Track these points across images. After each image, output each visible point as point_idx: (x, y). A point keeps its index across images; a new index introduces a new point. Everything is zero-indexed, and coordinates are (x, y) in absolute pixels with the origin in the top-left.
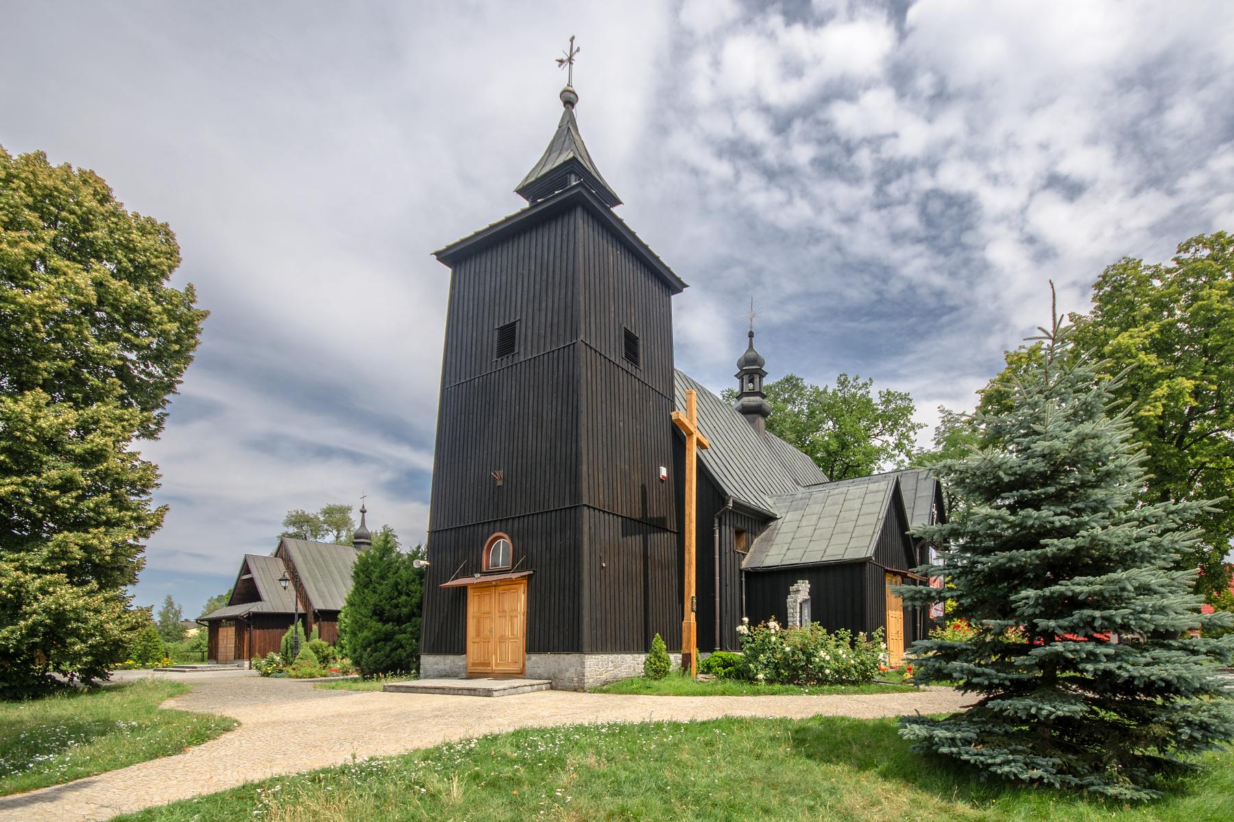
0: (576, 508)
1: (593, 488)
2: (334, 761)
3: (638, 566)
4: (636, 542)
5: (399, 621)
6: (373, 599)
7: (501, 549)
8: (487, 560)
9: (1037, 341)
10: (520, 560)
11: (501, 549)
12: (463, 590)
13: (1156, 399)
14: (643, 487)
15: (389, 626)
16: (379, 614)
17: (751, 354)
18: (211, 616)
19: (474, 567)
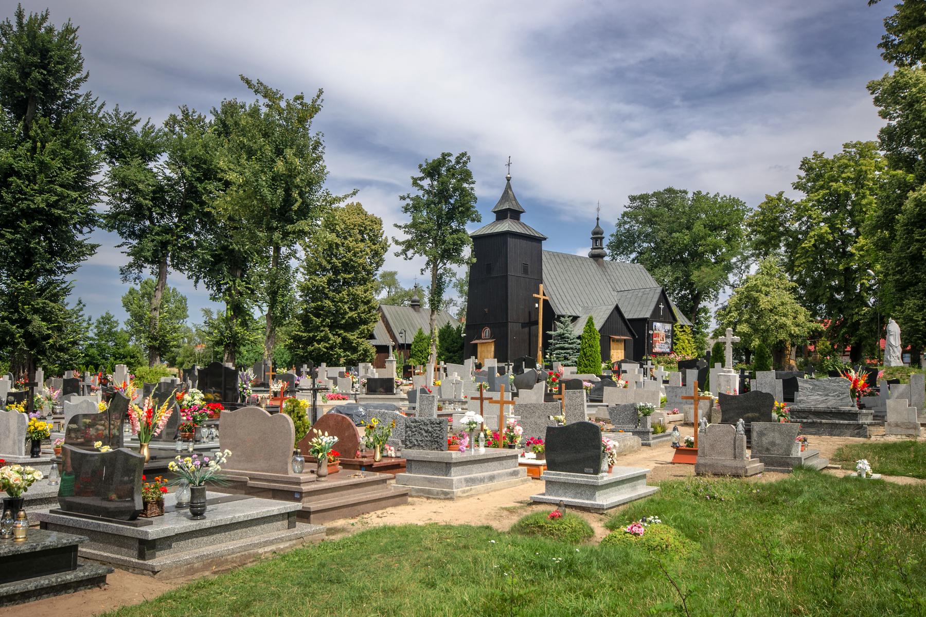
0: (507, 323)
1: (512, 314)
2: (632, 265)
3: (527, 337)
4: (526, 330)
5: (454, 352)
6: (446, 345)
7: (487, 332)
8: (483, 335)
9: (206, 523)
10: (492, 336)
11: (487, 332)
12: (476, 344)
13: (811, 237)
14: (529, 312)
15: (451, 354)
16: (447, 350)
17: (598, 229)
18: (768, 424)
19: (480, 338)
